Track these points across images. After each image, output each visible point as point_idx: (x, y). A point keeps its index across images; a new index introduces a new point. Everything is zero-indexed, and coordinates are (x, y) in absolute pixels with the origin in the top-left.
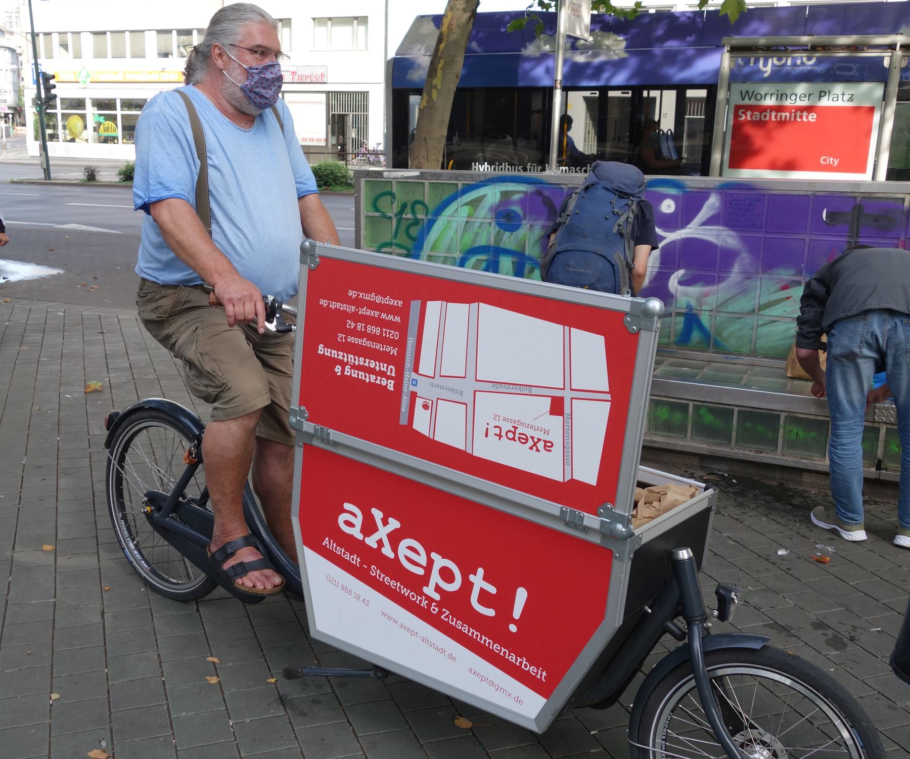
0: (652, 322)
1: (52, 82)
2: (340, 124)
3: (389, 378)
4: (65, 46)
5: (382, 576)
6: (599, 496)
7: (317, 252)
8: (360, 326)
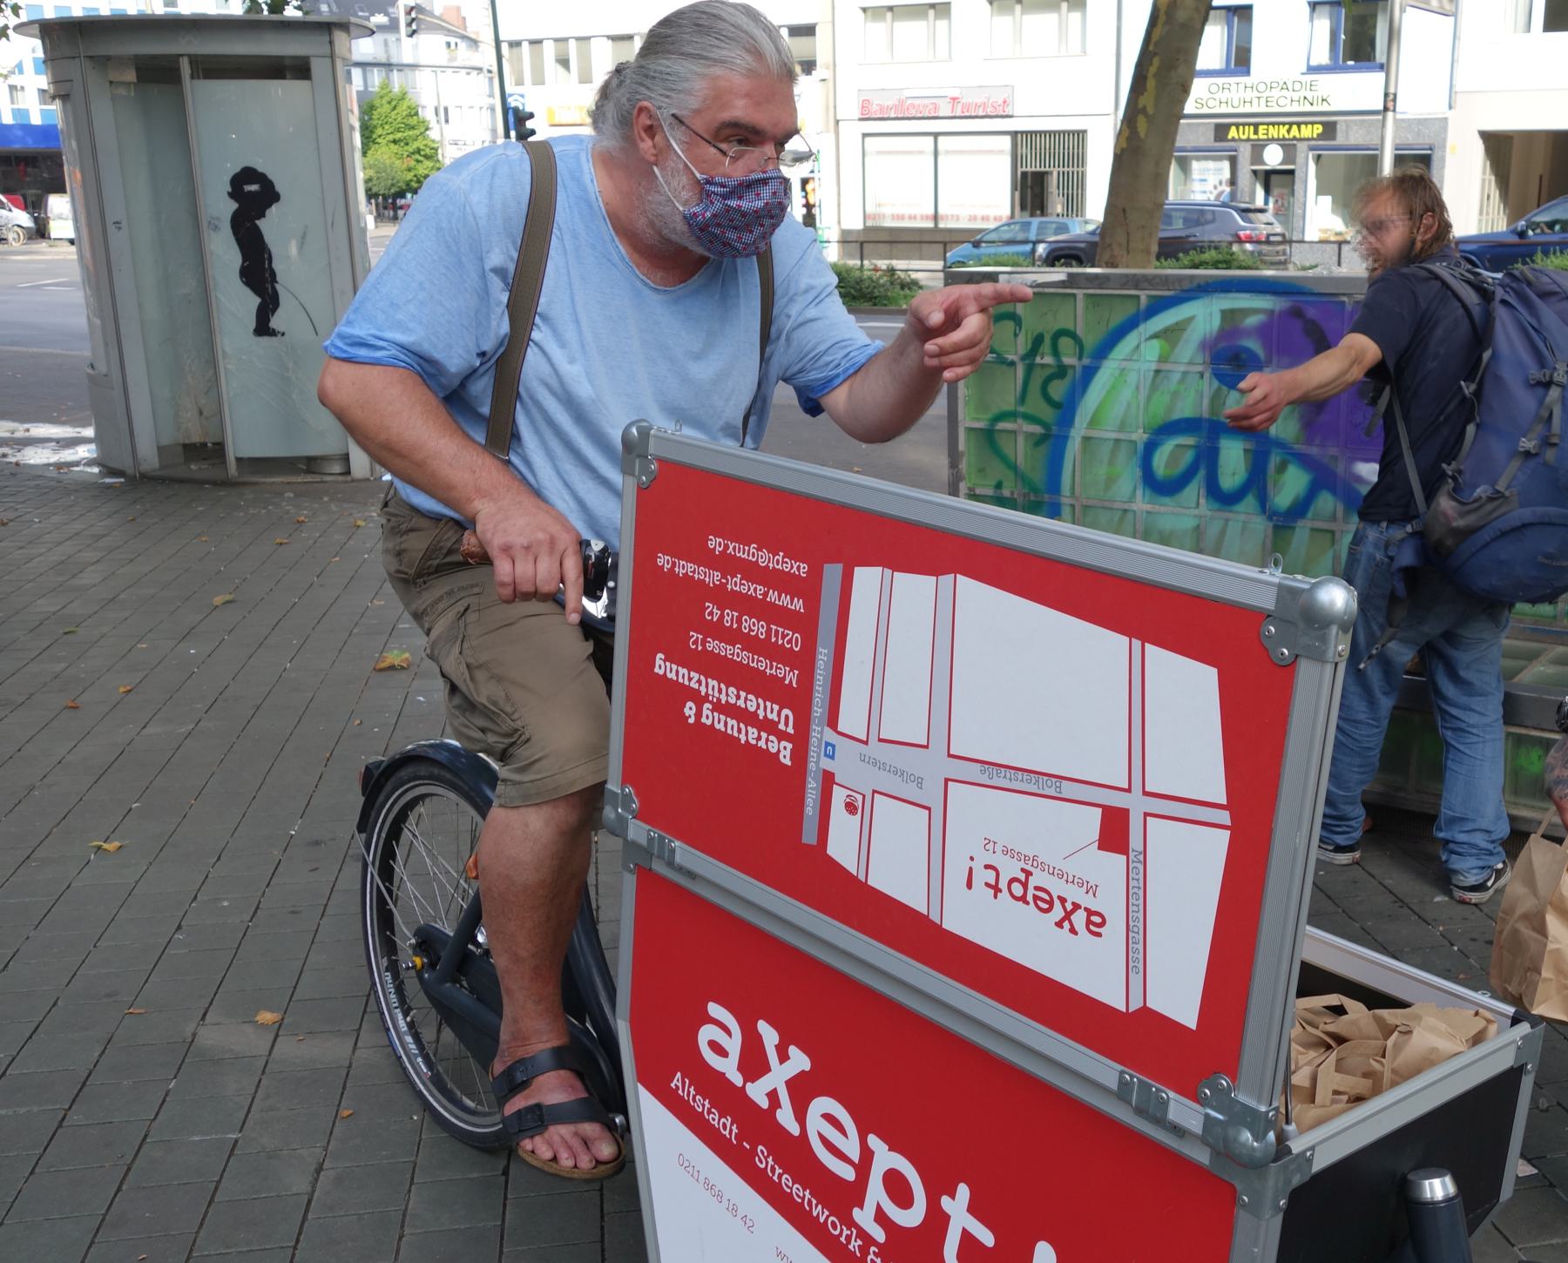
0: (1324, 639)
1: (529, 124)
2: (1037, 190)
3: (782, 736)
4: (564, 62)
5: (778, 1171)
6: (1200, 1055)
7: (651, 450)
8: (729, 617)
